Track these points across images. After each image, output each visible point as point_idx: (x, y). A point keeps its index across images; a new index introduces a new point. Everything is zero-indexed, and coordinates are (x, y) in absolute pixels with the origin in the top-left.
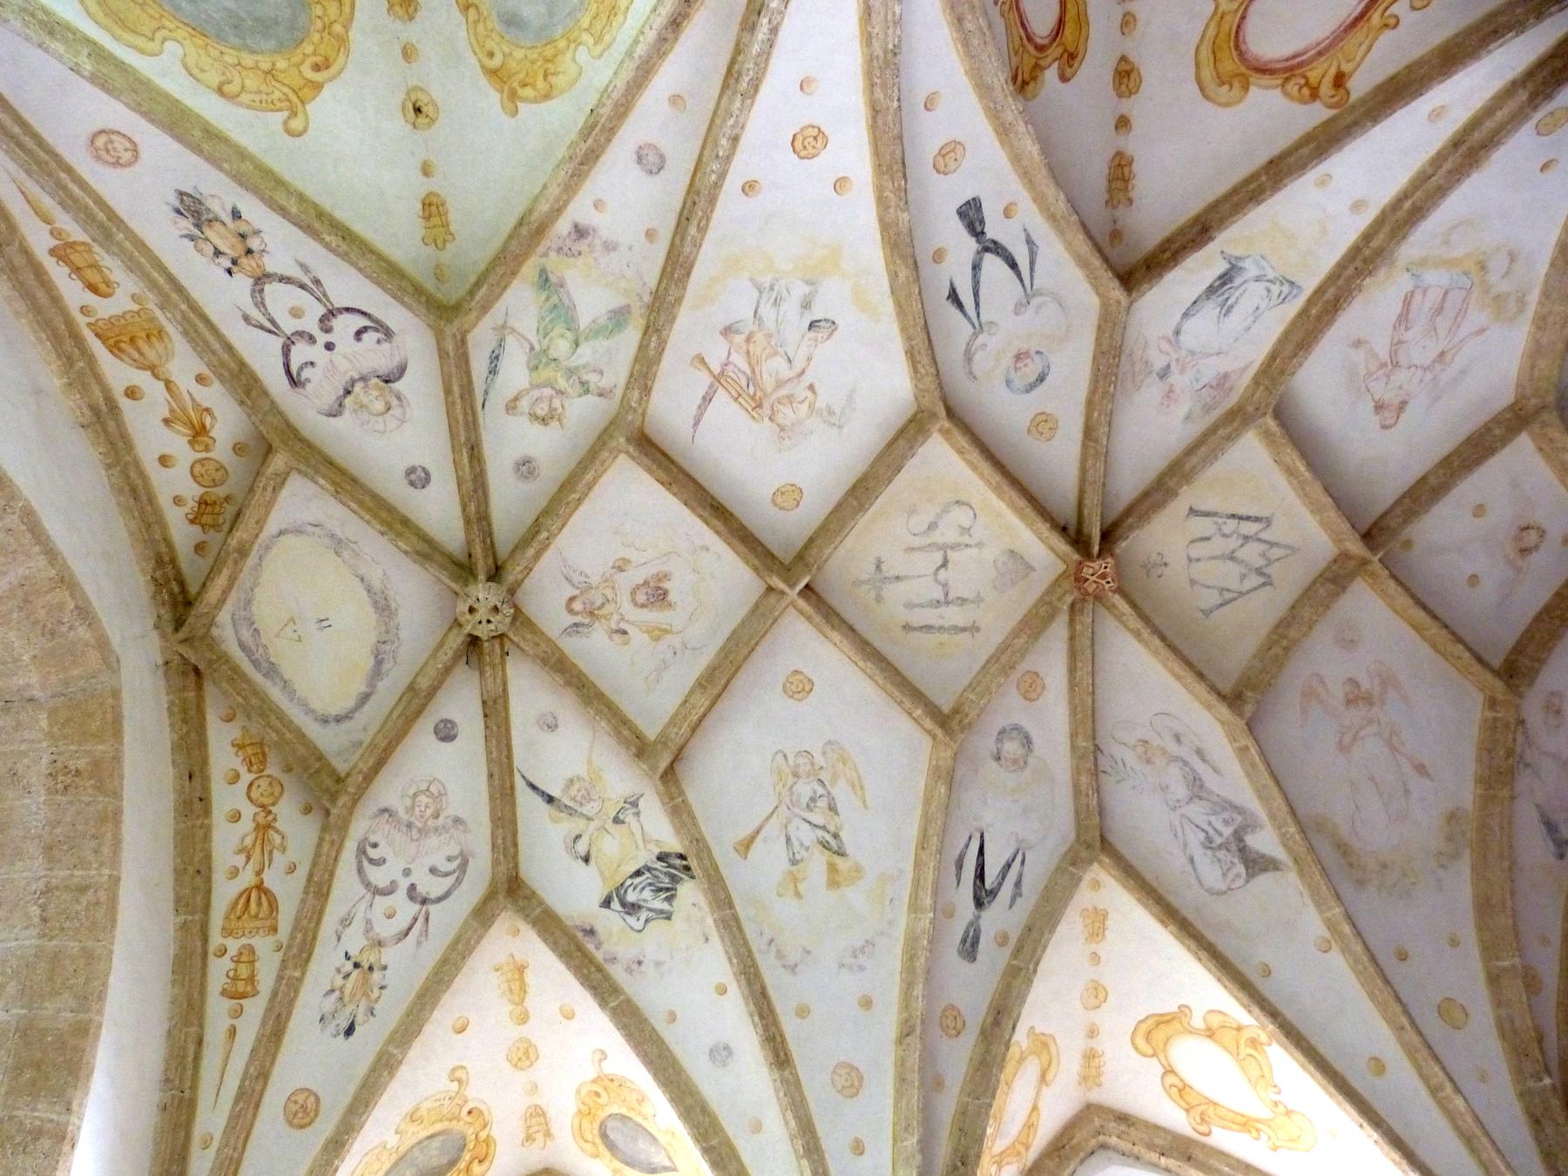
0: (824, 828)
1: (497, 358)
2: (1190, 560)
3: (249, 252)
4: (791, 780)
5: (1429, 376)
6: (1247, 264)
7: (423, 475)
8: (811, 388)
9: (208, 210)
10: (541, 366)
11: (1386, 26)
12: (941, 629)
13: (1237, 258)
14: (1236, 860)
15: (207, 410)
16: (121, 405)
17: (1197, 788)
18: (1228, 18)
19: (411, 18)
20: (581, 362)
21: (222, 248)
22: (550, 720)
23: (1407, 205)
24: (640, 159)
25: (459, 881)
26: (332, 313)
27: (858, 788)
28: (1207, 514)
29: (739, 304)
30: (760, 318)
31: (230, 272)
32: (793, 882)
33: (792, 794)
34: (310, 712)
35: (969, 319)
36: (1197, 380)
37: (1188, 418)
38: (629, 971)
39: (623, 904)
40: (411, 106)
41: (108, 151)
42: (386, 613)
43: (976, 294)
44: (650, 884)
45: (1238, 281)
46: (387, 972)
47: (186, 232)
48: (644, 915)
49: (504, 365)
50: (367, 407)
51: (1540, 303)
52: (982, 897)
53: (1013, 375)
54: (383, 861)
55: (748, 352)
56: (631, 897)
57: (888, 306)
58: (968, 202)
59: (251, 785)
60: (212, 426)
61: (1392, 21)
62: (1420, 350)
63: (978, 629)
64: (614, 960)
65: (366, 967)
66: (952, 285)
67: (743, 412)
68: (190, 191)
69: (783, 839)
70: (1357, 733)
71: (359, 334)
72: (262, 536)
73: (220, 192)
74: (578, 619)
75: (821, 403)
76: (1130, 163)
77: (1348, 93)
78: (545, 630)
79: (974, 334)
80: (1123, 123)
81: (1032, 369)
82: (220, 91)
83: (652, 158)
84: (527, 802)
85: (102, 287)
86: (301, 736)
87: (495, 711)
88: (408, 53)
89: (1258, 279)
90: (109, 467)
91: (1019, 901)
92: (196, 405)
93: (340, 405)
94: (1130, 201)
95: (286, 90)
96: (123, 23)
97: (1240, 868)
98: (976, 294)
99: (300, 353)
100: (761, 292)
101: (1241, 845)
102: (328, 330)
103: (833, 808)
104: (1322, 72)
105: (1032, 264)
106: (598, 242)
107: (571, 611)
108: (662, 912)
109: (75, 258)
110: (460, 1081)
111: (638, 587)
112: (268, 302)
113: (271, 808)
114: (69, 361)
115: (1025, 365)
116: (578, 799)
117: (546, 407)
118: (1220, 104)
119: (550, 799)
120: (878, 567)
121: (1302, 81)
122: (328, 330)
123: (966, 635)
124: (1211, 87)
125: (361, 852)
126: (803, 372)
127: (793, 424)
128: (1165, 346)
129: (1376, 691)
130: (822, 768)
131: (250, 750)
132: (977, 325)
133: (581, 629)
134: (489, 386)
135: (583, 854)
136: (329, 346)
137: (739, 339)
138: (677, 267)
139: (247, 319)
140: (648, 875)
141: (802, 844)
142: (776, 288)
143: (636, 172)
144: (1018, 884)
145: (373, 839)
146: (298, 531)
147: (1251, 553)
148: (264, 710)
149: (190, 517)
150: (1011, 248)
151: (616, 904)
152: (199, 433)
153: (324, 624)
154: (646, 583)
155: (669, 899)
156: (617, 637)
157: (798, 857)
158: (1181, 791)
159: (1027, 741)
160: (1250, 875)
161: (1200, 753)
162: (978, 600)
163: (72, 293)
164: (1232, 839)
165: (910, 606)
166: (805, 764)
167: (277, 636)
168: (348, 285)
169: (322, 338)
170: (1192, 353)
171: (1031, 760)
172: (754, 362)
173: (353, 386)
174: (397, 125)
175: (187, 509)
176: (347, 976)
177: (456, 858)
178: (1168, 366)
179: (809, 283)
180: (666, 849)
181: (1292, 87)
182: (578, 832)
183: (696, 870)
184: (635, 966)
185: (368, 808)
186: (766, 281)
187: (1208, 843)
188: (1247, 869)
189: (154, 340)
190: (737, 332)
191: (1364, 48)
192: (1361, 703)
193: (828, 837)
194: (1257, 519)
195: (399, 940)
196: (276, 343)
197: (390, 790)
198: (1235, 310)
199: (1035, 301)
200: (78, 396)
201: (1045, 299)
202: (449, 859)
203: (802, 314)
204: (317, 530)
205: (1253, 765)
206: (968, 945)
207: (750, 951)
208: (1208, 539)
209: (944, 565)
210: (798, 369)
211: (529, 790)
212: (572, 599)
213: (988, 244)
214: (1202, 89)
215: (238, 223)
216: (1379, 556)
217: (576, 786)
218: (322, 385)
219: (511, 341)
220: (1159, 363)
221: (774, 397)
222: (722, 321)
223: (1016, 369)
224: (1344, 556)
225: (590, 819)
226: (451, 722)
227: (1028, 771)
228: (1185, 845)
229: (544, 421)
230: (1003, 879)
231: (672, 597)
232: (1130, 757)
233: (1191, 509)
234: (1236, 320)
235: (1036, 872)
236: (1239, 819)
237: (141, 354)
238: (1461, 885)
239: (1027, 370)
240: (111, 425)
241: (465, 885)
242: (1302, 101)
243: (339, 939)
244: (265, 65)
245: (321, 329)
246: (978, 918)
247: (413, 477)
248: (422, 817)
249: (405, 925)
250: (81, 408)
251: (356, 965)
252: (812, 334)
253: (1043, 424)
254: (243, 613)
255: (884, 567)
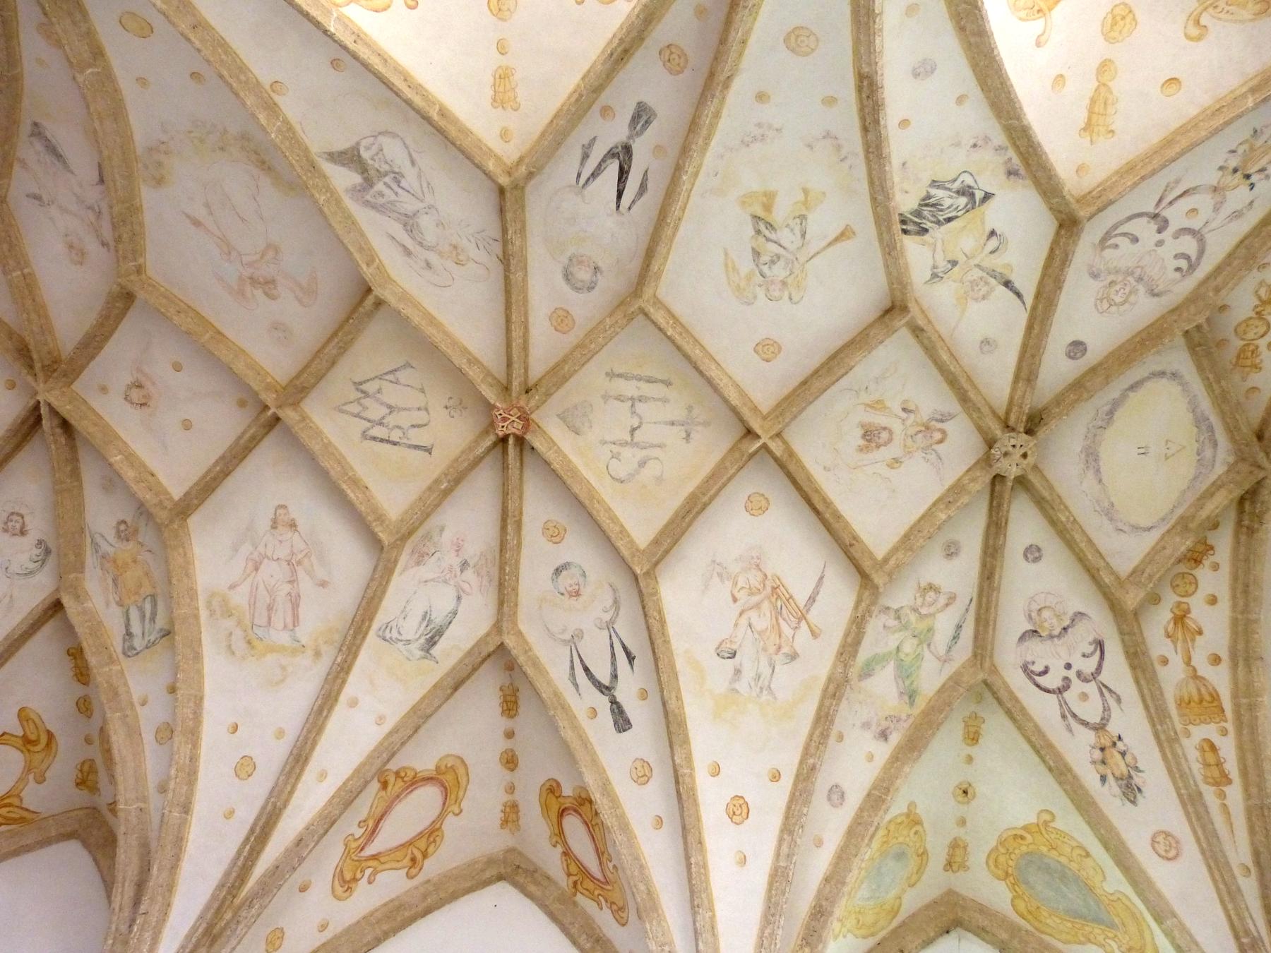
0: (768, 240)
1: (954, 638)
2: (426, 409)
3: (1102, 749)
4: (790, 280)
5: (261, 549)
6: (419, 653)
7: (1029, 555)
8: (735, 600)
9: (1120, 787)
10: (925, 631)
11: (364, 821)
12: (640, 379)
13: (425, 658)
14: (370, 162)
15: (1168, 636)
16: (1227, 653)
17: (409, 222)
18: (453, 802)
19: (955, 839)
20: (897, 635)
21: (1119, 757)
22: (986, 348)
23: (325, 714)
24: (842, 796)
25: (1115, 227)
26: (1060, 691)
27: (730, 265)
28: (416, 447)
29: (787, 679)
30: (770, 665)
31: (1120, 738)
32: (808, 199)
33: (791, 270)
34: (1185, 386)
35: (617, 635)
36: (439, 559)
37: (442, 529)
38: (987, 139)
39: (972, 195)
40: (969, 795)
41: (1170, 846)
42: (1091, 451)
43: (613, 655)
44: (942, 211)
45: (422, 640)
46: (1221, 163)
47: (1140, 774)
48: (957, 185)
49: (950, 631)
50: (1055, 615)
51: (197, 609)
52: (623, 154)
53: (581, 580)
54: (1176, 257)
55: (780, 636)
56: (963, 201)
57: (680, 664)
58: (624, 731)
59: (1262, 336)
60: (1169, 623)
61: (362, 824)
62: (273, 573)
63: (607, 374)
64: (999, 149)
65: (1239, 173)
66: (632, 668)
67: (786, 585)
68: (1128, 803)
69: (807, 236)
70: (262, 257)
71: (1045, 672)
72: (1164, 529)
73: (1108, 798)
74: (940, 425)
75: (729, 584)
76: (503, 712)
77: (379, 781)
78: (972, 424)
79: (613, 623)
80: (510, 735)
81: (566, 580)
82: (1088, 855)
83: (835, 797)
84: (1028, 283)
85: (1207, 748)
86: (1200, 369)
87: (1027, 369)
88: (962, 822)
89: (408, 642)
90: (1256, 621)
91: (586, 141)
92: (1175, 643)
93: (1073, 620)
94: (501, 689)
95: (1046, 836)
96: (1133, 915)
97: (365, 155)
98: (613, 655)
99: (1089, 666)
100: (769, 687)
101: (366, 175)
102: (1066, 679)
103: (756, 254)
104: (395, 787)
105: (572, 667)
106: (874, 727)
107: (943, 432)
108: (938, 187)
109: (1216, 773)
110: (1197, 22)
111: (885, 444)
112: (1101, 709)
113: (1254, 315)
114: (1252, 707)
115: (571, 586)
116: (982, 283)
117: (928, 598)
118: (452, 755)
119: (1007, 284)
120: (688, 435)
121: (405, 779)
122: (1066, 679)
123: (618, 370)
124: (458, 763)
125: (1192, 267)
126: (741, 614)
127: (750, 569)
128: (466, 586)
129: (248, 288)
130: (760, 286)
131: (1248, 362)
132: (611, 630)
133: (939, 417)
134: (964, 615)
135: (994, 238)
136: (1068, 666)
137: (785, 650)
138: (824, 720)
139: (1119, 700)
140: (941, 218)
141: (792, 230)
142: (758, 690)
143: (845, 786)
144: (586, 156)
145: (1178, 275)
146: (1136, 528)
147: (376, 412)
148: (1222, 399)
149: (1212, 552)
150: (589, 683)
151: (979, 195)
152: (1181, 618)
153: (1142, 451)
154: (878, 447)
155: (929, 197)
156: (912, 407)
157: (798, 221)
158: (425, 222)
159: (568, 276)
160: (356, 148)
161: (408, 253)
162: (606, 397)
163: (1228, 749)
164: (375, 180)
165: (665, 401)
166: (774, 290)
167: (1184, 447)
168: (1043, 709)
169: (1072, 674)
170: (445, 582)
171: (566, 261)
172: (776, 627)
173: (1060, 633)
174: (980, 788)
175: (1212, 559)
176: (1262, 170)
177: (1109, 247)
178: (462, 571)
179: (735, 691)
180: (918, 238)
181: (411, 774)
182: (992, 256)
183: (897, 218)
184: (980, 143)
185: (1167, 302)
186: (765, 696)
187: (398, 177)
188: (359, 156)
189: (1186, 699)
190: (787, 655)
191: (374, 806)
192: (261, 280)
193: (767, 233)
194: (374, 438)
195: (1194, 189)
196: (1104, 677)
197: (1145, 310)
198: (420, 618)
199: (567, 636)
200: (1256, 684)
201: (561, 636)
202: (1116, 246)
203: (741, 665)
204: (1120, 525)
205: (361, 249)
206: (644, 118)
207: (867, 158)
208: (413, 426)
209: (633, 430)
210: (745, 616)
211: (1022, 292)
212: (941, 441)
213: (606, 692)
214: (463, 761)
215: (1103, 773)
216: (270, 413)
217: (981, 293)
218: (1082, 637)
219: (942, 651)
220: (469, 574)
221: (762, 595)
222: (796, 664)
223: (578, 584)
224: (295, 405)
225: (978, 266)
226: (1070, 357)
227: (569, 254)
228: (419, 177)
229: (931, 587)
230: (600, 164)
231: (860, 432)
232: (473, 252)
233: (430, 453)
234: (417, 610)
235: (567, 166)
236: (368, 197)
237: (1199, 690)
238: (142, 128)
239: (569, 581)
240: (1241, 646)
241: (1110, 223)
242: (404, 768)
243: (1252, 202)
244: (1054, 854)
245: (1070, 680)
246: (630, 137)
247: (1037, 555)
248: (1126, 284)
249: (1182, 200)
250: (1258, 675)
251: (1248, 177)
252: (735, 647)
253: (555, 535)
254: (1203, 471)
255: (684, 435)
